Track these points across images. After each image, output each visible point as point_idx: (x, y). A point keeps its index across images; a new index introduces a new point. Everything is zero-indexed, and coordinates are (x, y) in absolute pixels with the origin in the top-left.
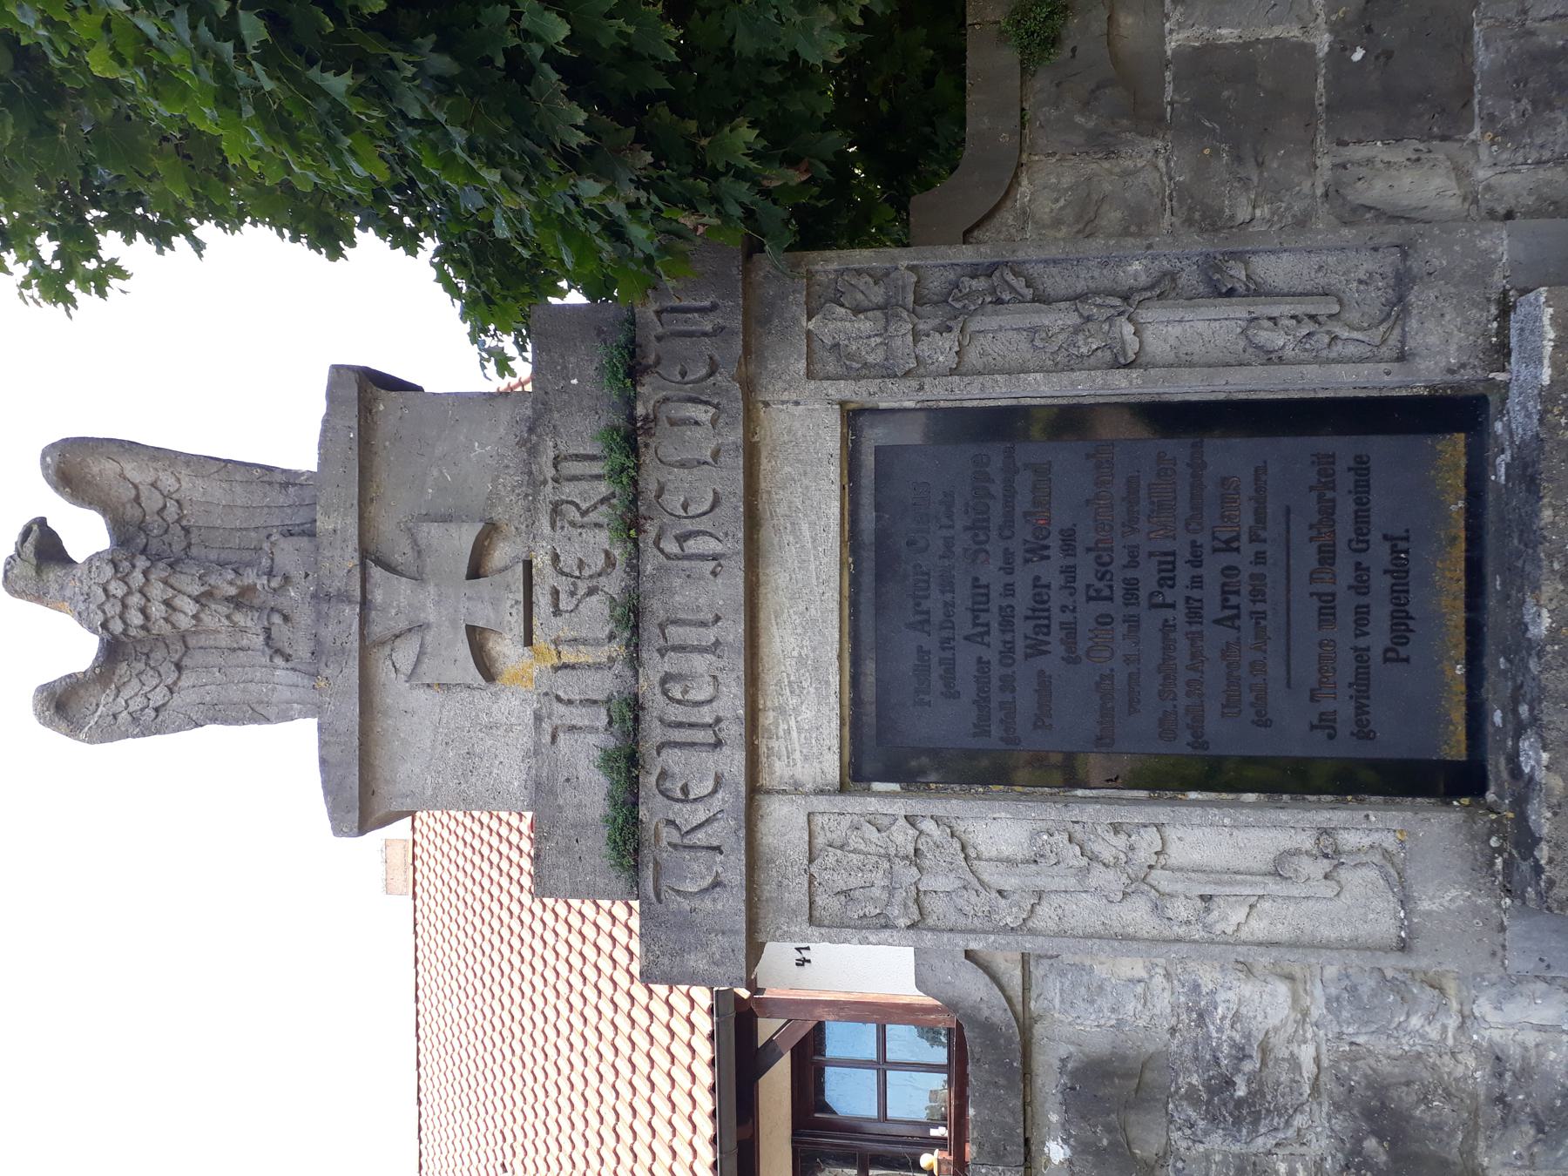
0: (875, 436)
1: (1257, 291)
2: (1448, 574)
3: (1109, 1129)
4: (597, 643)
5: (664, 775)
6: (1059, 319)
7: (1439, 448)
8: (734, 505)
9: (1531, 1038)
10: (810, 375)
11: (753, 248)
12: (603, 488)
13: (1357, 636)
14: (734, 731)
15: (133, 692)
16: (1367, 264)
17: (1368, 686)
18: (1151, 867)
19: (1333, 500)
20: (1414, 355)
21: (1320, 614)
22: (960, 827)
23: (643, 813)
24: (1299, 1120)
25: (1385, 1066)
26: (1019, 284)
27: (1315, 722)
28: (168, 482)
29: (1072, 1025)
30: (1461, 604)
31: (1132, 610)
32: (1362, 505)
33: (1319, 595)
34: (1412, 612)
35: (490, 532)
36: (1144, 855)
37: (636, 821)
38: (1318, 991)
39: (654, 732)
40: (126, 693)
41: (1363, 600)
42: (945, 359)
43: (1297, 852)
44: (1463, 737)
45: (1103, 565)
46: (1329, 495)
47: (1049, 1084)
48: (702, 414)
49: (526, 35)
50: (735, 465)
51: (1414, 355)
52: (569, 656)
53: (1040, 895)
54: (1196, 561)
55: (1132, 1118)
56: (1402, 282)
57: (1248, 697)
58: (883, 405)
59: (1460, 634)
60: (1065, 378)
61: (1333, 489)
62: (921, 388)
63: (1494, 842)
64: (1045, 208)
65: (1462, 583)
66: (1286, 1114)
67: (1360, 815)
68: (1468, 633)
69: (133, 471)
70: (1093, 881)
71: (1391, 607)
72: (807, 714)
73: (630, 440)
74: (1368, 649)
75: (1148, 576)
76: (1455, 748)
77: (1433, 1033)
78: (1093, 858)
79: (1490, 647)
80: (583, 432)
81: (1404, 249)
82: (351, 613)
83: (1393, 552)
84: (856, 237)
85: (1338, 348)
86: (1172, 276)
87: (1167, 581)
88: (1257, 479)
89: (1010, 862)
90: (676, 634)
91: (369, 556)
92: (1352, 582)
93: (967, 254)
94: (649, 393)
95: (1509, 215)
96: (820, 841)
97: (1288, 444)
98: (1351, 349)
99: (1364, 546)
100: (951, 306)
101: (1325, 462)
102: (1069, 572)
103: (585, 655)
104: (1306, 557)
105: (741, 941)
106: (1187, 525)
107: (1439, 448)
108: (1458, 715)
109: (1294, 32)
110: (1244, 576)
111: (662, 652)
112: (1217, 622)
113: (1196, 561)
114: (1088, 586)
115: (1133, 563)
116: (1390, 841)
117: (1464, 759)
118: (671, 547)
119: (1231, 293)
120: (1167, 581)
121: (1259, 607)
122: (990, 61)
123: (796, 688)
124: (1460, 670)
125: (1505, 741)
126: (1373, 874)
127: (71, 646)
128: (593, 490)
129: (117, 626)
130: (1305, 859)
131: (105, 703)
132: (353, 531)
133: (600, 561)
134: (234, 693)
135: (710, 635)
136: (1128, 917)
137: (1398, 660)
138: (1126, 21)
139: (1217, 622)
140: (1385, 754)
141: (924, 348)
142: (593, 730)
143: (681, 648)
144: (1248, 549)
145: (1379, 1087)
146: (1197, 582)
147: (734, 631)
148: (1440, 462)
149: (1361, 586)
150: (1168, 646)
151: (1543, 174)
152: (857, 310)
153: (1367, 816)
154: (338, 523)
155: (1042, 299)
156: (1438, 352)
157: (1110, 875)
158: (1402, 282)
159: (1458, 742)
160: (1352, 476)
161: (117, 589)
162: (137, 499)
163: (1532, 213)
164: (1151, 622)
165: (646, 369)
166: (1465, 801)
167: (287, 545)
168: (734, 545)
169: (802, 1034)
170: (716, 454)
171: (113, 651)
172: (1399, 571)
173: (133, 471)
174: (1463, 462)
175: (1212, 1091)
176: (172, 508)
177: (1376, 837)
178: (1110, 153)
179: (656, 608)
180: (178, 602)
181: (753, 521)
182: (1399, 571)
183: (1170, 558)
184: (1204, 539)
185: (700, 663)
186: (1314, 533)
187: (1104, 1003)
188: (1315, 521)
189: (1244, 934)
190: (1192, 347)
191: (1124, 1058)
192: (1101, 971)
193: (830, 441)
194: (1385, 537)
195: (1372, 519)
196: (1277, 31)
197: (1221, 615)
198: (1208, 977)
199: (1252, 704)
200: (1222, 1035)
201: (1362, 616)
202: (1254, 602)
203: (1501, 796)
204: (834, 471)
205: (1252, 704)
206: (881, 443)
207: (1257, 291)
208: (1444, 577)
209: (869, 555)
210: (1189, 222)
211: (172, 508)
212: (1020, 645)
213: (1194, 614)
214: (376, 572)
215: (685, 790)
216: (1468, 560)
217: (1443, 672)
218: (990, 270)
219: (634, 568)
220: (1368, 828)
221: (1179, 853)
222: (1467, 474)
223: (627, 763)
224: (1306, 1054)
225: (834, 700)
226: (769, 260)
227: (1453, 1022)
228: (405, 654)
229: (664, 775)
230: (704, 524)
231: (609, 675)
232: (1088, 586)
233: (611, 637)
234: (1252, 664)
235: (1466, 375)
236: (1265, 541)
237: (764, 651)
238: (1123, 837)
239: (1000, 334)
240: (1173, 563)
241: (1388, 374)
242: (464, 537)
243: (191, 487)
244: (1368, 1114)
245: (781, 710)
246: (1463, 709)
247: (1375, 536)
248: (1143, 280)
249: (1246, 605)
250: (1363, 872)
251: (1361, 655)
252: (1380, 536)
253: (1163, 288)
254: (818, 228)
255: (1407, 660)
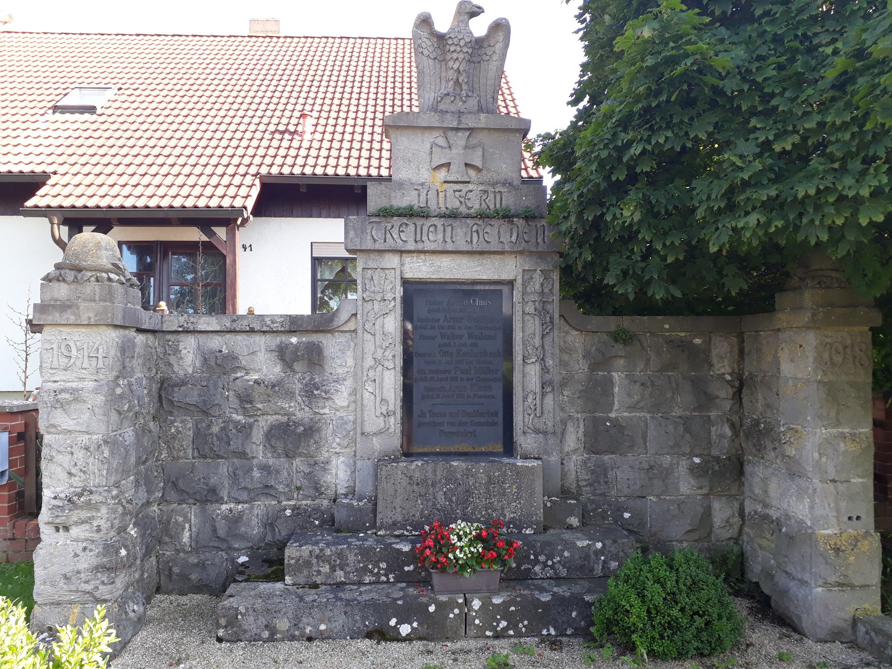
0: (506, 290)
1: (543, 395)
3: (303, 355)
4: (445, 203)
5: (407, 225)
6: (537, 341)
8: (487, 248)
9: (334, 471)
10: (524, 270)
11: (561, 255)
12: (492, 207)
14: (420, 246)
15: (427, 44)
16: (550, 424)
22: (392, 313)
23: (395, 218)
24: (307, 409)
25: (324, 432)
26: (547, 330)
28: (495, 57)
29: (331, 344)
35: (478, 170)
36: (387, 364)
37: (393, 216)
38: (344, 414)
39: (419, 222)
40: (427, 41)
42: (527, 310)
47: (314, 338)
48: (514, 238)
49: (608, 208)
50: (498, 248)
52: (441, 195)
53: (374, 335)
54: (468, 380)
55: (306, 362)
56: (545, 433)
57: (430, 394)
59: (448, 450)
60: (521, 343)
64: (569, 339)
66: (310, 406)
69: (499, 46)
70: (378, 349)
72: (424, 268)
73: (507, 216)
77: (334, 445)
78: (385, 350)
80: (509, 201)
81: (554, 433)
82: (454, 124)
84: (564, 284)
85: (527, 416)
86: (548, 372)
89: (383, 327)
90: (449, 229)
91: (472, 130)
93: (556, 316)
94: (520, 222)
95: (562, 464)
96: (387, 271)
98: (527, 420)
100: (542, 311)
101: (496, 415)
102: (465, 345)
103: (441, 200)
105: (358, 248)
108: (426, 450)
109: (616, 408)
111: (443, 225)
116: (392, 430)
118: (474, 228)
119: (543, 388)
122: (612, 323)
123: (432, 265)
127: (442, 25)
128: (492, 203)
129: (450, 42)
131: (424, 34)
132: (480, 126)
133: (470, 205)
134: (427, 79)
135: (448, 240)
136: (368, 359)
138: (621, 362)
141: (530, 303)
142: (419, 202)
143: (444, 231)
145: (319, 430)
146: (462, 380)
147: (450, 247)
149: (461, 424)
150: (444, 372)
151: (574, 473)
152: (542, 284)
154: (483, 120)
155: (543, 336)
156: (525, 441)
157: (381, 355)
158: (545, 433)
161: (462, 43)
162: (490, 46)
163: (563, 470)
165: (527, 222)
167: (476, 102)
168: (475, 247)
169: (220, 248)
170: (502, 242)
171: (441, 37)
173: (499, 46)
175: (314, 384)
176: (487, 58)
177: (393, 426)
178: (584, 357)
179: (457, 223)
180: (457, 62)
181: (481, 253)
185: (440, 236)
187: (339, 354)
189: (365, 391)
190: (527, 378)
191: (323, 359)
192: (349, 353)
193: (505, 276)
196: (616, 403)
198: (349, 383)
200: (332, 387)
204: (496, 277)
207: (543, 395)
209: (470, 288)
210: (564, 379)
211: (487, 58)
212: (444, 331)
213: (453, 379)
214: (467, 134)
215: (402, 231)
218: (552, 322)
219: (468, 216)
220: (395, 424)
221: (387, 373)
223: (409, 213)
224: (327, 411)
225: (428, 276)
226: (556, 258)
227: (337, 450)
228: (441, 141)
229: (407, 225)
230: (481, 238)
231: (435, 207)
233: (447, 208)
235: (519, 449)
237: (442, 255)
239: (534, 325)
242: (478, 163)
243: (493, 66)
244: (311, 428)
245: (425, 260)
248: (547, 364)
250: (383, 423)
251: (442, 424)
253: (545, 370)
254: (566, 271)
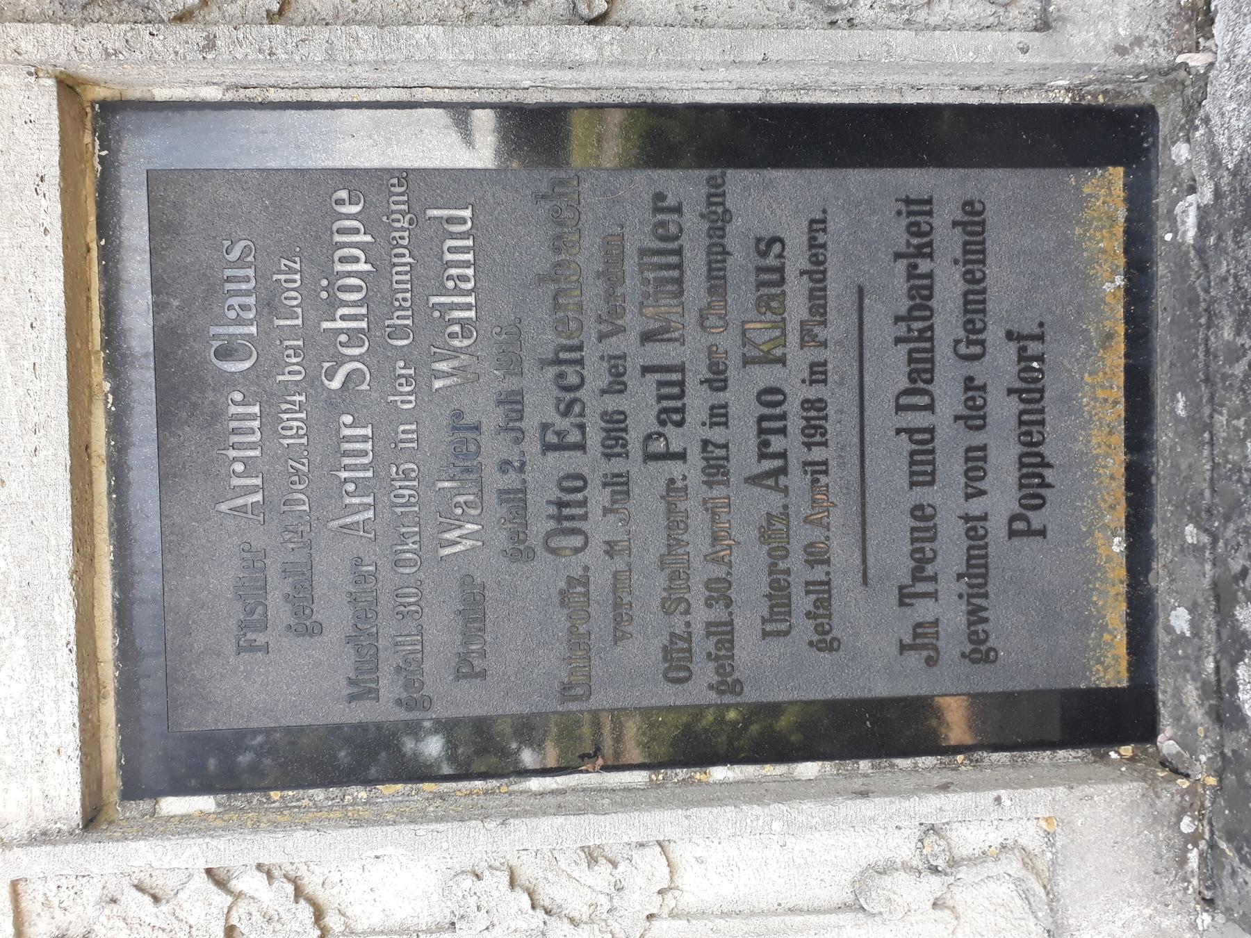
2: (1101, 394)
7: (1086, 190)
13: (968, 497)
17: (985, 576)
18: (650, 917)
19: (930, 276)
20: (1062, 19)
21: (912, 463)
27: (908, 640)
30: (1119, 439)
31: (617, 465)
32: (974, 281)
33: (910, 431)
34: (1050, 459)
41: (978, 439)
43: (884, 870)
44: (1122, 650)
45: (568, 389)
46: (924, 266)
51: (1062, 19)
57: (802, 602)
58: (161, 94)
59: (1117, 489)
61: (930, 256)
62: (210, 44)
63: (1187, 825)
65: (1121, 407)
67: (988, 797)
68: (1129, 486)
71: (1019, 449)
74: (984, 518)
75: (640, 405)
76: (1112, 671)
79: (1163, 507)
83: (1021, 359)
87: (671, 414)
88: (813, 244)
92: (961, 410)
97: (859, 179)
99: (976, 350)
101: (917, 209)
102: (513, 402)
104: (890, 370)
106: (702, 318)
107: (1086, 190)
108: (1116, 615)
110: (793, 407)
112: (754, 480)
113: (717, 380)
114: (545, 427)
115: (617, 385)
116: (1031, 837)
117: (1125, 684)
120: (671, 414)
121: (817, 454)
124: (1118, 545)
125: (1198, 660)
126: (1004, 891)
130: (901, 876)
137: (1030, 533)
139: (754, 480)
140: (1018, 684)
144: (799, 358)
146: (719, 416)
148: (1088, 214)
149: (974, 417)
150: (675, 523)
153: (998, 800)
159: (1116, 659)
160: (958, 236)
164: (649, 482)
166: (1127, 750)
172: (1030, 390)
174: (1122, 214)
182: (1030, 390)
183: (675, 377)
184: (728, 342)
186: (902, 330)
188: (903, 311)
194: (1010, 335)
195: (990, 306)
197: (757, 470)
199: (808, 615)
201: (976, 460)
202: (809, 446)
203: (1189, 745)
205: (808, 615)
206: (157, 164)
208: (1095, 399)
209: (143, 379)
213: (716, 469)
216: (1128, 370)
217: (1093, 550)
221: (697, 888)
222: (1125, 232)
232: (545, 427)
234: (809, 548)
235: (1143, 56)
236: (824, 344)
238: (604, 868)
240: (681, 384)
241: (1024, 51)
246: (1124, 607)
247: (995, 334)
249: (792, 443)
251: (974, 526)
252: (1001, 334)
255: (1042, 533)
